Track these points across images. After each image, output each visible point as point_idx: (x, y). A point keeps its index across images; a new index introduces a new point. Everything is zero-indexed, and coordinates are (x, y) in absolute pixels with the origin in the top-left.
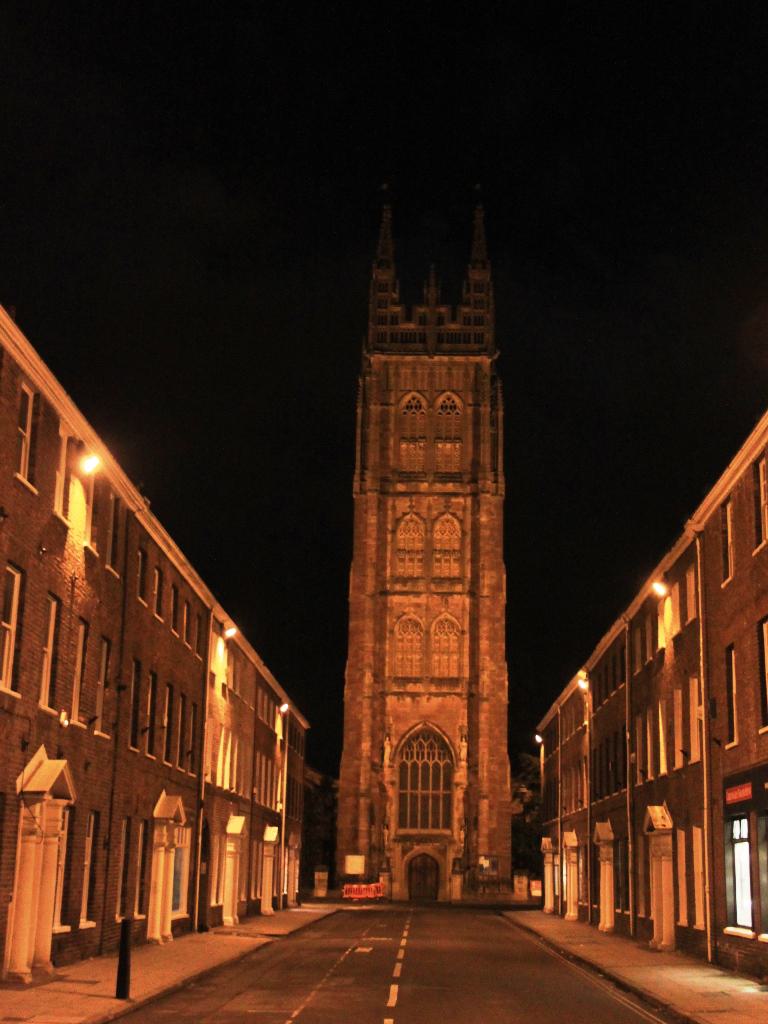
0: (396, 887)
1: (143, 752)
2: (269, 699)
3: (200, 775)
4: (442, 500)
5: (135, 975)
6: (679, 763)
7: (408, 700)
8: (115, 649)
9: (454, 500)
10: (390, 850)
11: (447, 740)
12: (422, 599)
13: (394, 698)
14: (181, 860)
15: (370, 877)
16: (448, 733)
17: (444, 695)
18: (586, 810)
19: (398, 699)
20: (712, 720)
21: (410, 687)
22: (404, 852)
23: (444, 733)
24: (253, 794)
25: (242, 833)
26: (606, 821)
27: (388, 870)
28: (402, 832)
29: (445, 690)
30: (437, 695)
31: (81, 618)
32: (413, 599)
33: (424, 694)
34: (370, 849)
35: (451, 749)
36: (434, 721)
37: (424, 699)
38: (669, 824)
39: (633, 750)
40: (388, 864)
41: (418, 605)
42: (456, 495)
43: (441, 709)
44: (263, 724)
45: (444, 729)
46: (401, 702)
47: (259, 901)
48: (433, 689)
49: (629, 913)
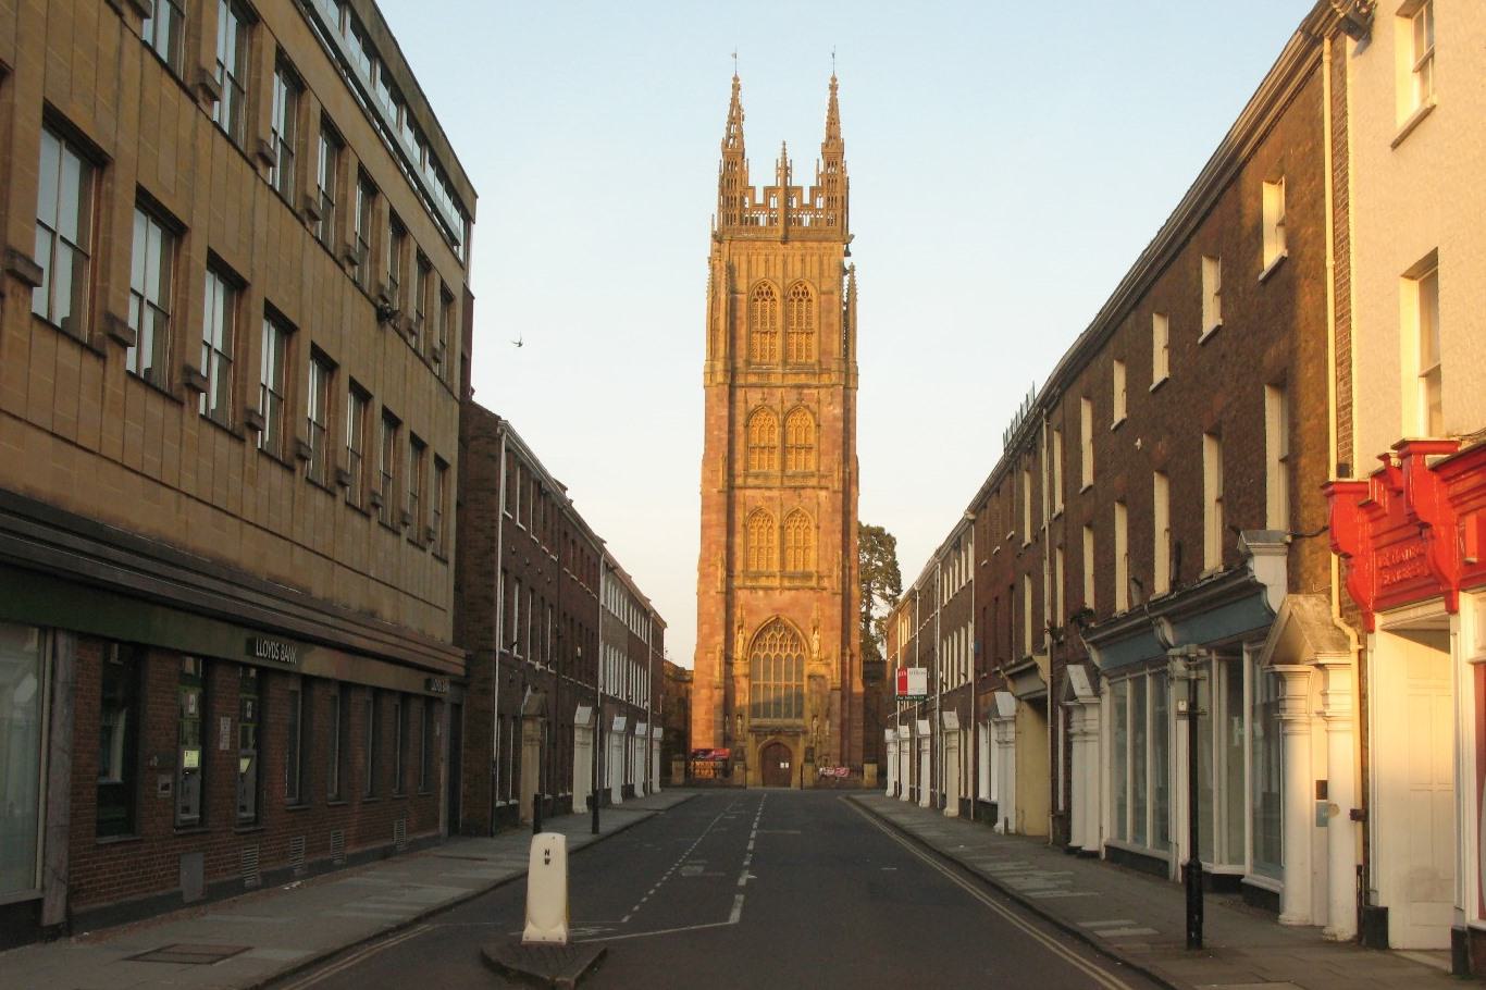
0: (750, 775)
1: (526, 659)
2: (628, 602)
3: (597, 688)
4: (795, 391)
5: (601, 820)
6: (963, 681)
7: (761, 593)
8: (555, 610)
9: (806, 391)
10: (744, 740)
12: (775, 493)
13: (746, 592)
14: (1065, 789)
15: (246, 699)
16: (802, 627)
17: (797, 589)
18: (970, 684)
20: (1434, 414)
21: (763, 582)
22: (757, 742)
23: (797, 626)
24: (628, 696)
25: (589, 724)
26: (953, 710)
27: (743, 759)
28: (756, 721)
29: (797, 583)
30: (789, 589)
31: (517, 578)
32: (767, 493)
33: (777, 589)
34: (725, 740)
35: (804, 641)
36: (787, 615)
37: (777, 592)
38: (957, 725)
39: (941, 670)
40: (743, 753)
41: (770, 499)
42: (809, 387)
43: (794, 603)
44: (635, 636)
47: (633, 786)
48: (786, 583)
49: (938, 791)
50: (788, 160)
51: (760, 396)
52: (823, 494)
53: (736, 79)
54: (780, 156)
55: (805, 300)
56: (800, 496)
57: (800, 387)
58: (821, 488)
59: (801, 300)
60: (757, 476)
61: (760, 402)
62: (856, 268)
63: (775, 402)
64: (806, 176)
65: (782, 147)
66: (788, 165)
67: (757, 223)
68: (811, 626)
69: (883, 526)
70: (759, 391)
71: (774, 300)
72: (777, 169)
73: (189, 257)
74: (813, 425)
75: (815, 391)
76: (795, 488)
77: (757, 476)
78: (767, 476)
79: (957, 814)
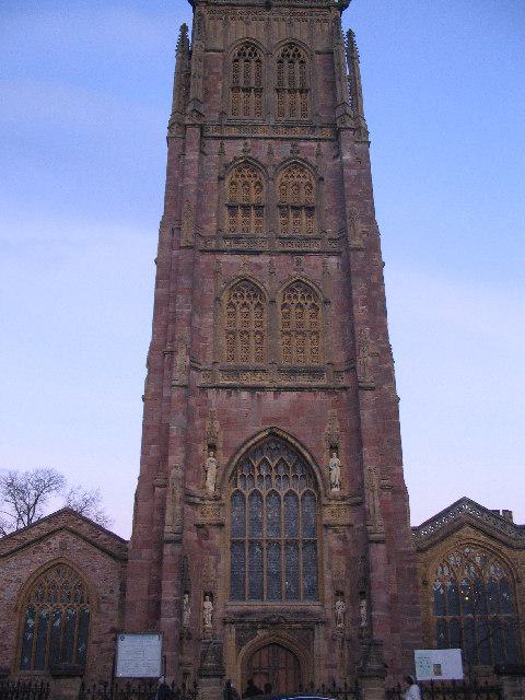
9: (302, 144)
11: (306, 455)
19: (229, 394)
30: (288, 389)
32: (254, 259)
41: (259, 266)
45: (301, 439)
46: (233, 398)
52: (333, 260)
56: (298, 263)
58: (330, 254)
60: (237, 239)
63: (262, 156)
68: (325, 445)
70: (241, 142)
71: (258, 61)
75: (314, 144)
76: (294, 253)
77: (237, 239)
78: (252, 239)
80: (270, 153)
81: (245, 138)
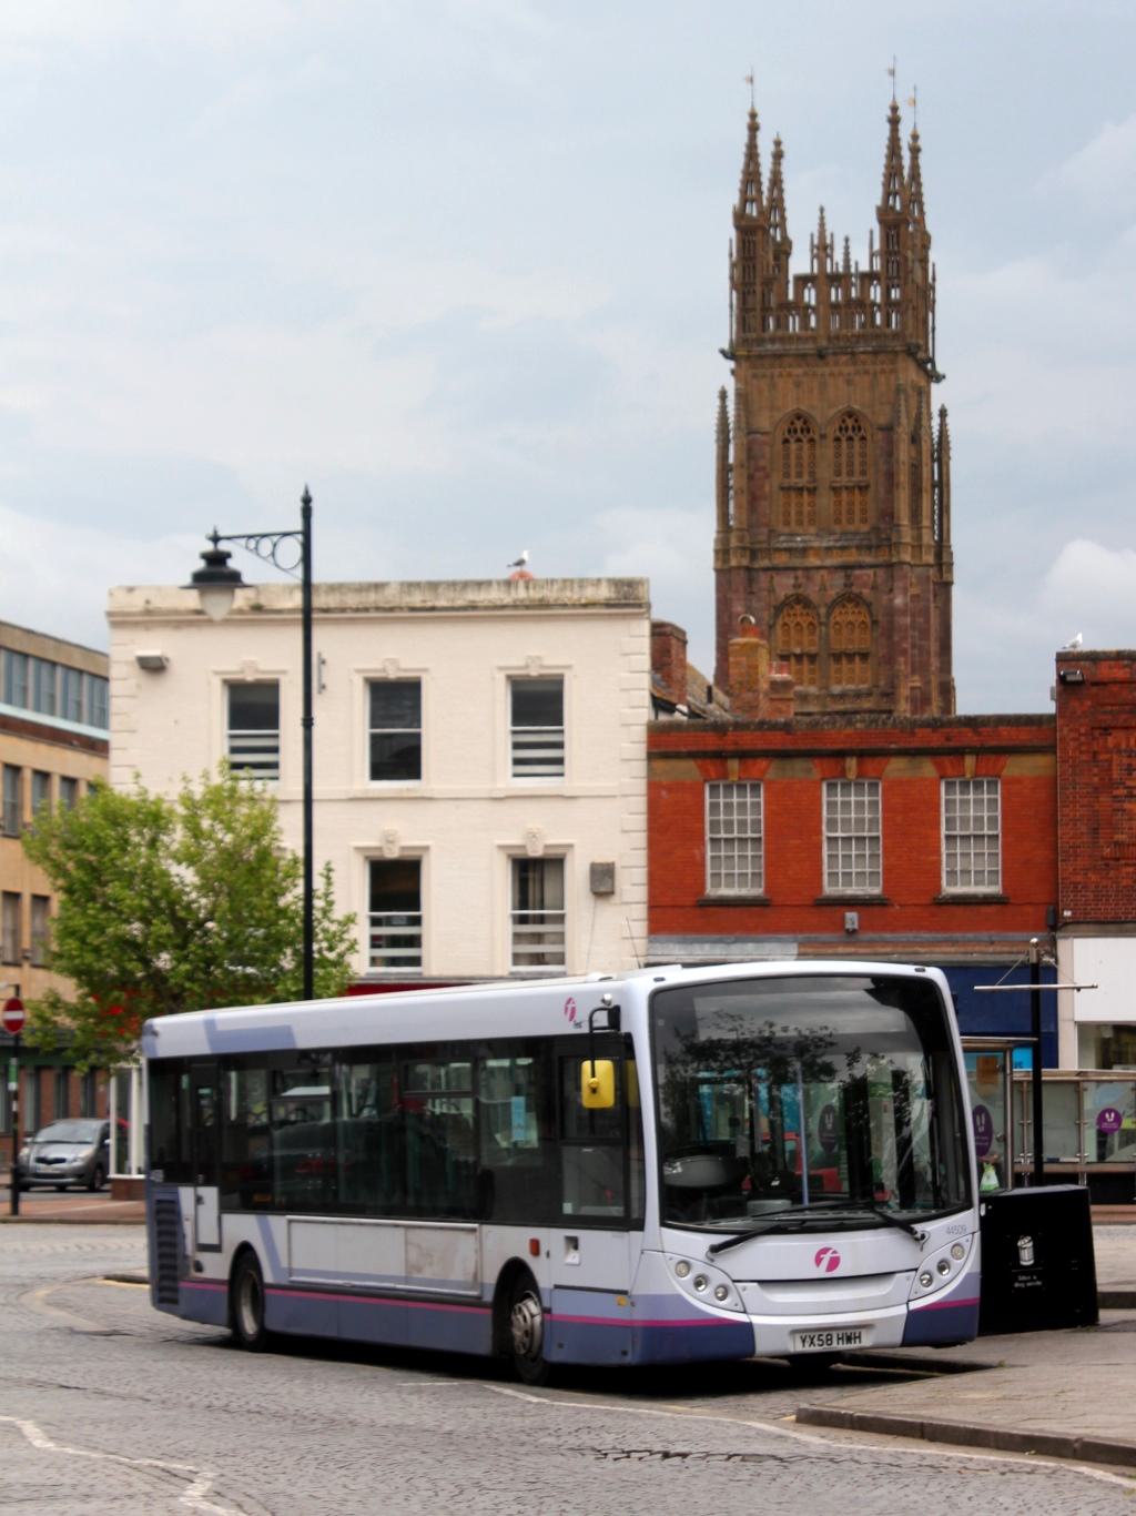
9: (857, 572)
42: (861, 566)
50: (828, 234)
51: (792, 581)
53: (753, 116)
54: (815, 229)
55: (856, 438)
57: (846, 568)
59: (850, 439)
61: (791, 591)
62: (949, 412)
63: (812, 591)
64: (860, 248)
65: (818, 214)
66: (828, 241)
67: (918, 596)
69: (729, 373)
70: (792, 574)
72: (812, 246)
73: (402, 584)
74: (868, 621)
79: (997, 1185)
80: (823, 588)
81: (794, 569)
